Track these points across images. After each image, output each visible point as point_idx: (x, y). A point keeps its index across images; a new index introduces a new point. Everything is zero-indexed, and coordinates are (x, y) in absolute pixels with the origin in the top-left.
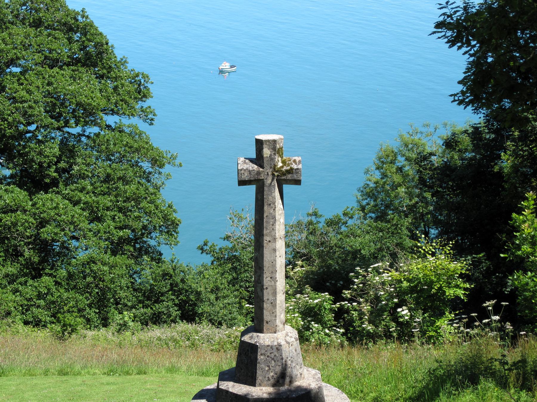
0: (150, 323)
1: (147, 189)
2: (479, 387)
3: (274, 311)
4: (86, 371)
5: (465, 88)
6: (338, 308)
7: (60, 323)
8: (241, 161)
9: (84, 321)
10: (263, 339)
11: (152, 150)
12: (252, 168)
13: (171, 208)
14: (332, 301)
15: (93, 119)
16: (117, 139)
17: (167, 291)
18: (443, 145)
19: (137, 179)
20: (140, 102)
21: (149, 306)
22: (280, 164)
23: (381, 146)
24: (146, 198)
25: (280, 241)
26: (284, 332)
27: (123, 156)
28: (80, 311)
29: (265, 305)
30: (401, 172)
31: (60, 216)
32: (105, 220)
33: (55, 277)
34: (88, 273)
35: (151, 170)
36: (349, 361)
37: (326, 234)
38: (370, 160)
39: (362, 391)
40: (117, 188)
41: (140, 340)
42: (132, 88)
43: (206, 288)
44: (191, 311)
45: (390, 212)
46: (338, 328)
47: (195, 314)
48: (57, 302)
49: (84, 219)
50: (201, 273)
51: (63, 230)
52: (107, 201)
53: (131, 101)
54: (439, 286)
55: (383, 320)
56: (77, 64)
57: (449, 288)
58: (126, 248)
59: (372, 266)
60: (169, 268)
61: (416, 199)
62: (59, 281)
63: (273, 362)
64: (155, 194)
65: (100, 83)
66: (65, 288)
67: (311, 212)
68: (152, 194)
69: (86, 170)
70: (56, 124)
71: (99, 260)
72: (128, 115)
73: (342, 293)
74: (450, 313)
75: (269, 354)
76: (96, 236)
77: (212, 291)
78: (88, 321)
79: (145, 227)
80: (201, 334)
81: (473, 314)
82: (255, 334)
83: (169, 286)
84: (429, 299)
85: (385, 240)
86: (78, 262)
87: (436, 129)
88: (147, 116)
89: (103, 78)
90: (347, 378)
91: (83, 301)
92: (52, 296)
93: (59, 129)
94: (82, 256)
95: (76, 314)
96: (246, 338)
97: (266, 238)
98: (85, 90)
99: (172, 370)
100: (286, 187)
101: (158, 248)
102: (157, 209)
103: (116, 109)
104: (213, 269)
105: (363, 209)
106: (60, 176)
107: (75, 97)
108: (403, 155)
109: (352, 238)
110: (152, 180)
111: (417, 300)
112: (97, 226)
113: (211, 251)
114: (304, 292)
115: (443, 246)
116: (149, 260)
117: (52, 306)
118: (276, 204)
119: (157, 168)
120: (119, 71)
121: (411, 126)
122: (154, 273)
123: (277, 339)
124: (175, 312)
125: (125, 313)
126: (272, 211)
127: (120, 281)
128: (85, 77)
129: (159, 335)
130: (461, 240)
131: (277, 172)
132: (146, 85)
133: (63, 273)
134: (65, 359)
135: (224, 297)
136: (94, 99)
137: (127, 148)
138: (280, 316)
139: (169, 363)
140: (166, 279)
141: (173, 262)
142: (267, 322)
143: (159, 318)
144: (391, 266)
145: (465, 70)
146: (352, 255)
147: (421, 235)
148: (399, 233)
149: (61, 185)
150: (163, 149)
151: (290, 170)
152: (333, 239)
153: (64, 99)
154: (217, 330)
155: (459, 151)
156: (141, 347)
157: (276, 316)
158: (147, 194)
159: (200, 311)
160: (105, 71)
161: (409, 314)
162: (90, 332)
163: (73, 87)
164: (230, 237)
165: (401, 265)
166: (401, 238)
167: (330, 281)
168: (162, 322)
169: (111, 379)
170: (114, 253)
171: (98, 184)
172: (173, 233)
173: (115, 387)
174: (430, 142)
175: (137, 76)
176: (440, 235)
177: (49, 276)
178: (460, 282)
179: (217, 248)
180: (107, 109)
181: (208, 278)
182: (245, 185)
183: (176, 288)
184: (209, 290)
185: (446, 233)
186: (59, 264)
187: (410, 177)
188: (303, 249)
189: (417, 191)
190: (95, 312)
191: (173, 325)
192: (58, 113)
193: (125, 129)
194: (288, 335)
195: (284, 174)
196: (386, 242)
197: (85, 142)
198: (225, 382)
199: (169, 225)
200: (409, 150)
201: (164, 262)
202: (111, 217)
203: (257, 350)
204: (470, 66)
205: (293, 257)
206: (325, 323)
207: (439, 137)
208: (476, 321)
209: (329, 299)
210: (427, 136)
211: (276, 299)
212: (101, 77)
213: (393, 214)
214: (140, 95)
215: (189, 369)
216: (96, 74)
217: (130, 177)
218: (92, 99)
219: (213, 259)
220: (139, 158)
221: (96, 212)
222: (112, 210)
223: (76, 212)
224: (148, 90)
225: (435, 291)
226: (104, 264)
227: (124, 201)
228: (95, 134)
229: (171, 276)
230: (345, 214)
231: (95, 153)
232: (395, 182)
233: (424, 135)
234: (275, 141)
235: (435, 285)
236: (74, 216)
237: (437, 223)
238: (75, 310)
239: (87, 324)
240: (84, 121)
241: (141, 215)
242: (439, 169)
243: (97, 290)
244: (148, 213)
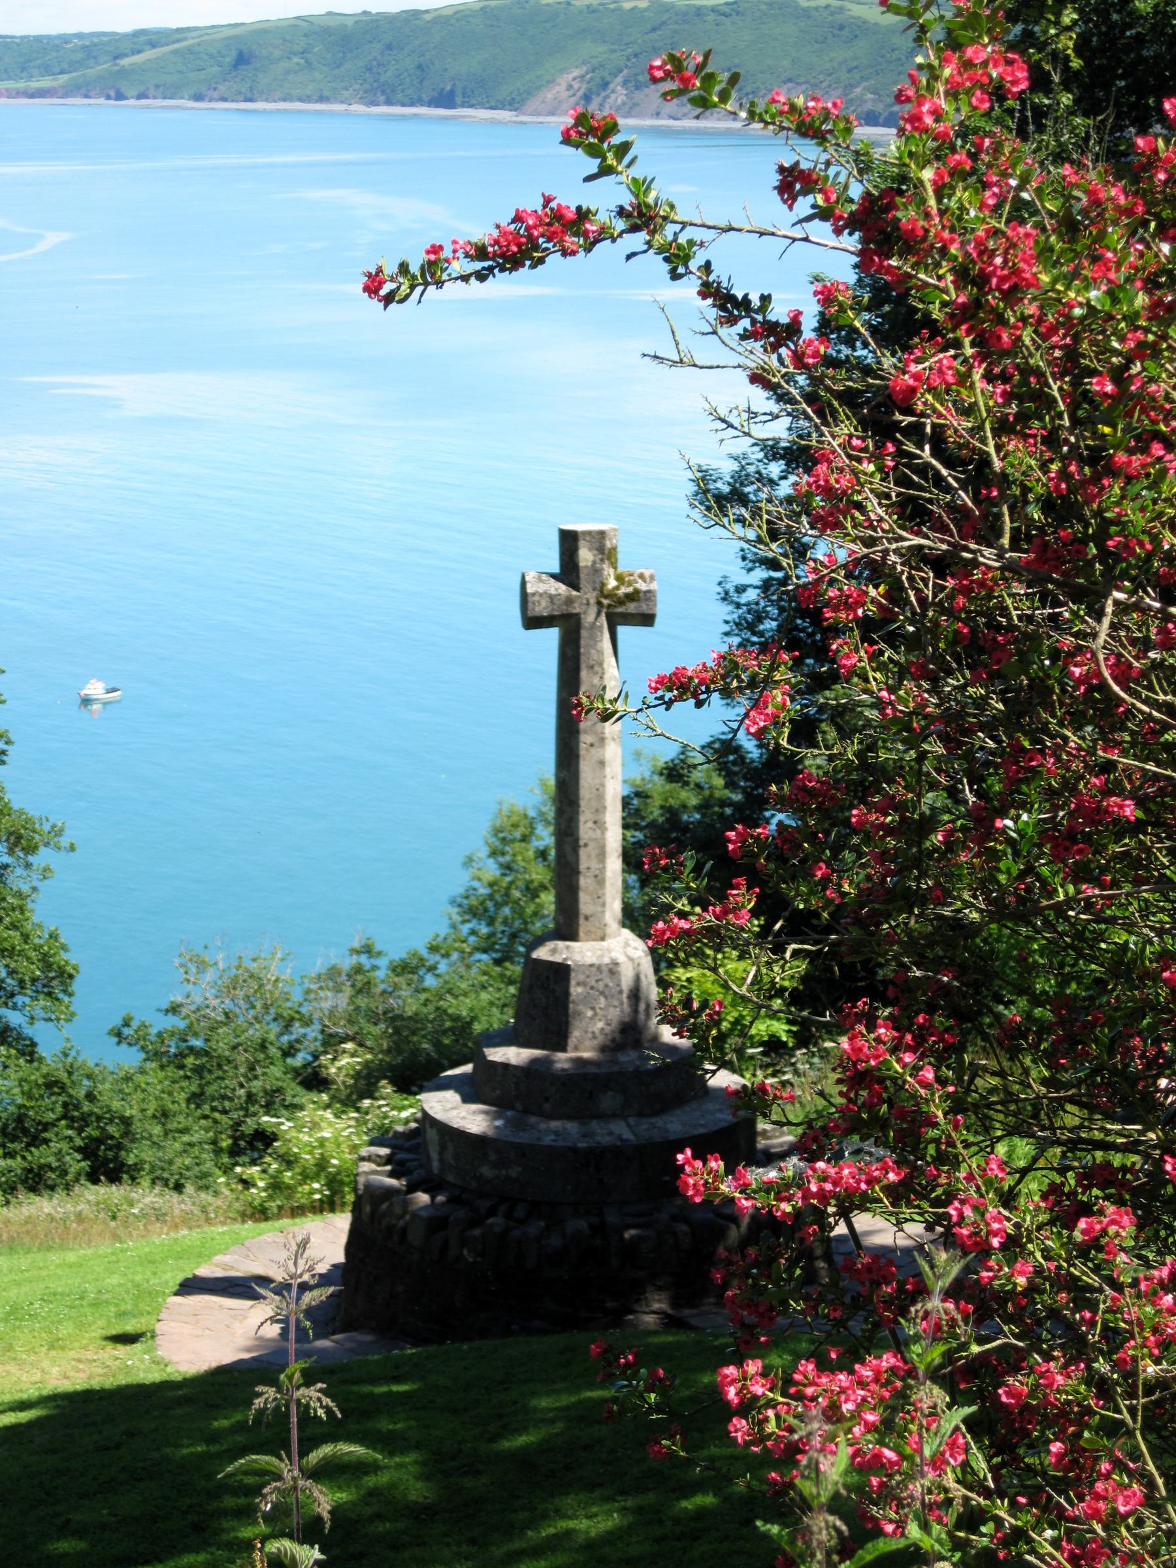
10: (578, 953)
22: (612, 583)
44: (111, 1161)
54: (735, 1014)
63: (602, 999)
67: (356, 945)
75: (593, 983)
82: (561, 944)
83: (59, 1109)
100: (622, 630)
123: (609, 951)
124: (76, 1164)
126: (596, 681)
131: (606, 597)
141: (66, 1055)
142: (587, 918)
150: (33, 813)
157: (604, 905)
159: (131, 1160)
195: (621, 602)
219: (143, 1056)
229: (63, 1088)
234: (602, 534)
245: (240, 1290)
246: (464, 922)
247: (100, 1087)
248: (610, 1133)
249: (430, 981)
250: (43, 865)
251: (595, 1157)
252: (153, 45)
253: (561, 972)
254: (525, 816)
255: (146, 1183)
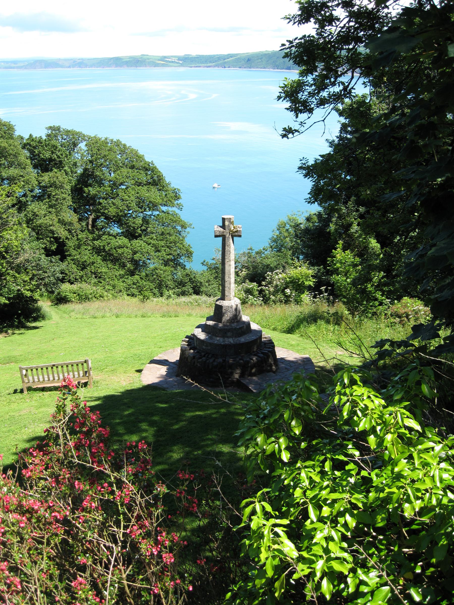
22: (232, 228)
100: (235, 238)
124: (191, 291)
195: (234, 233)
249: (263, 255)
251: (225, 346)
252: (232, 57)
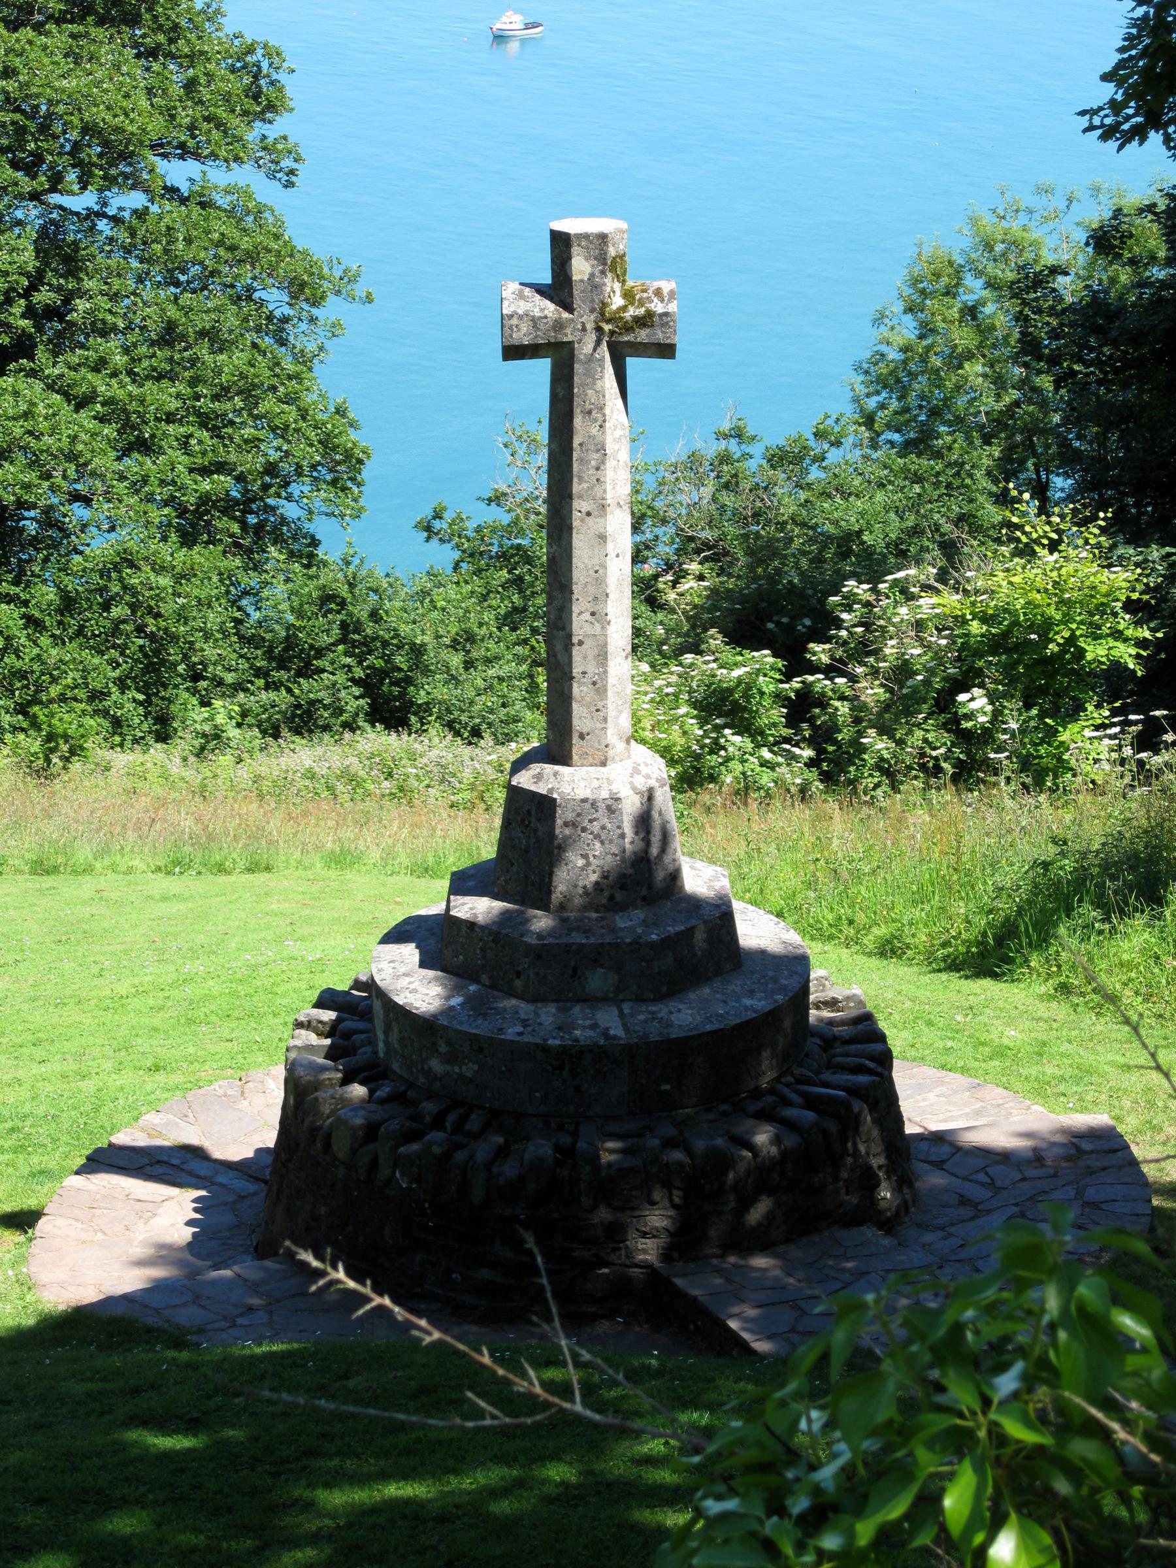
0: (285, 732)
1: (278, 364)
2: (1168, 914)
3: (600, 705)
4: (107, 861)
5: (1121, 92)
6: (797, 692)
7: (40, 729)
8: (510, 291)
9: (106, 723)
10: (568, 783)
11: (291, 256)
12: (542, 310)
13: (344, 416)
14: (782, 674)
15: (128, 170)
16: (195, 226)
17: (333, 644)
18: (1087, 244)
19: (250, 337)
20: (258, 124)
21: (282, 684)
22: (618, 302)
23: (920, 246)
24: (274, 388)
25: (618, 511)
26: (628, 764)
27: (212, 274)
28: (96, 696)
29: (576, 690)
30: (974, 318)
31: (37, 438)
32: (161, 447)
33: (26, 603)
34: (117, 594)
35: (287, 311)
36: (818, 838)
37: (766, 488)
38: (889, 287)
39: (851, 922)
40: (193, 361)
41: (257, 779)
42: (237, 85)
43: (438, 637)
44: (395, 699)
45: (943, 429)
46: (797, 745)
47: (409, 706)
48: (32, 672)
49: (103, 446)
50: (425, 593)
51: (47, 476)
52: (166, 396)
53: (234, 121)
54: (1066, 634)
55: (919, 725)
56: (83, 18)
57: (1096, 638)
58: (219, 526)
59: (889, 578)
60: (337, 581)
61: (1015, 394)
62: (37, 614)
63: (598, 845)
64: (297, 377)
65: (148, 69)
66: (53, 636)
67: (726, 426)
68: (290, 377)
69: (110, 311)
70: (26, 184)
71: (146, 559)
72: (226, 160)
73: (806, 650)
74: (1098, 706)
76: (137, 492)
77: (455, 645)
78: (117, 724)
79: (271, 469)
80: (425, 760)
81: (1157, 713)
82: (549, 768)
83: (336, 632)
84: (1039, 669)
85: (929, 506)
86: (90, 565)
87: (1070, 201)
88: (277, 163)
89: (156, 59)
90: (811, 885)
91: (103, 670)
92: (18, 657)
93: (35, 196)
94: (100, 547)
95: (83, 706)
96: (524, 780)
97: (580, 505)
98: (106, 91)
99: (342, 859)
100: (633, 364)
101: (306, 526)
102: (304, 418)
103: (191, 143)
104: (457, 583)
105: (869, 420)
106: (40, 328)
107: (80, 110)
108: (979, 273)
109: (838, 499)
110: (291, 338)
111: (1008, 670)
112: (141, 464)
113: (454, 535)
114: (703, 647)
115: (1078, 525)
116: (282, 557)
117: (18, 685)
118: (607, 411)
119: (305, 306)
120: (200, 38)
121: (1002, 193)
122: (297, 593)
123: (610, 782)
124: (353, 701)
125: (217, 703)
126: (594, 431)
127: (204, 617)
128: (107, 55)
129: (308, 763)
130: (1137, 505)
131: (608, 321)
132: (275, 76)
133: (47, 594)
134: (50, 829)
135: (488, 661)
136: (132, 115)
137: (221, 251)
138: (617, 717)
139: (334, 842)
140: (330, 611)
141: (348, 563)
142: (582, 736)
143: (310, 717)
144: (942, 577)
145: (1121, 44)
146: (839, 546)
147: (1021, 493)
148: (967, 486)
149: (41, 354)
150: (320, 253)
151: (644, 317)
152: (787, 500)
153: (49, 115)
154: (467, 751)
155: (1132, 262)
156: (261, 796)
157: (605, 720)
158: (277, 376)
160: (161, 38)
161: (989, 708)
162: (121, 756)
163: (74, 83)
164: (505, 494)
165: (969, 574)
166: (971, 501)
167: (775, 618)
168: (317, 727)
169: (172, 885)
170: (188, 539)
171: (143, 350)
172: (349, 484)
173: (183, 907)
174: (1055, 236)
175: (250, 50)
176: (1080, 489)
177: (8, 603)
178: (1124, 621)
179: (471, 525)
180: (169, 143)
181: (444, 609)
182: (522, 358)
183: (356, 637)
184: (447, 641)
185: (1096, 487)
186: (37, 569)
187: (999, 334)
188: (703, 529)
189: (1018, 371)
190: (134, 700)
191: (347, 735)
192: (31, 154)
193: (217, 197)
194: (639, 772)
195: (628, 328)
196: (931, 510)
197: (109, 233)
198: (467, 899)
199: (338, 463)
200: (995, 260)
201: (325, 564)
202: (177, 440)
203: (555, 812)
204: (1134, 31)
205: (678, 552)
206: (762, 733)
207: (1078, 224)
208: (1166, 732)
209: (772, 668)
210: (1046, 219)
211: (606, 672)
212: (152, 53)
213: (949, 433)
214: (259, 104)
215: (389, 855)
216: (136, 45)
217: (231, 331)
218: (127, 115)
220: (254, 278)
221: (134, 427)
222: (180, 421)
223: (82, 426)
224: (280, 90)
225: (1056, 649)
226: (159, 569)
227: (216, 398)
228: (135, 212)
229: (343, 604)
230: (819, 435)
231: (135, 264)
232: (956, 346)
233: (1036, 216)
234: (603, 238)
235: (1057, 633)
236: (76, 437)
237: (1068, 459)
238: (81, 694)
239: (114, 733)
240: (104, 178)
241: (261, 434)
242: (1075, 312)
243: (141, 642)
244: (282, 431)
245: (159, 1169)
246: (868, 395)
247: (387, 605)
248: (594, 1026)
250: (333, 319)
251: (571, 1060)
253: (544, 806)
254: (951, 263)
255: (435, 729)
